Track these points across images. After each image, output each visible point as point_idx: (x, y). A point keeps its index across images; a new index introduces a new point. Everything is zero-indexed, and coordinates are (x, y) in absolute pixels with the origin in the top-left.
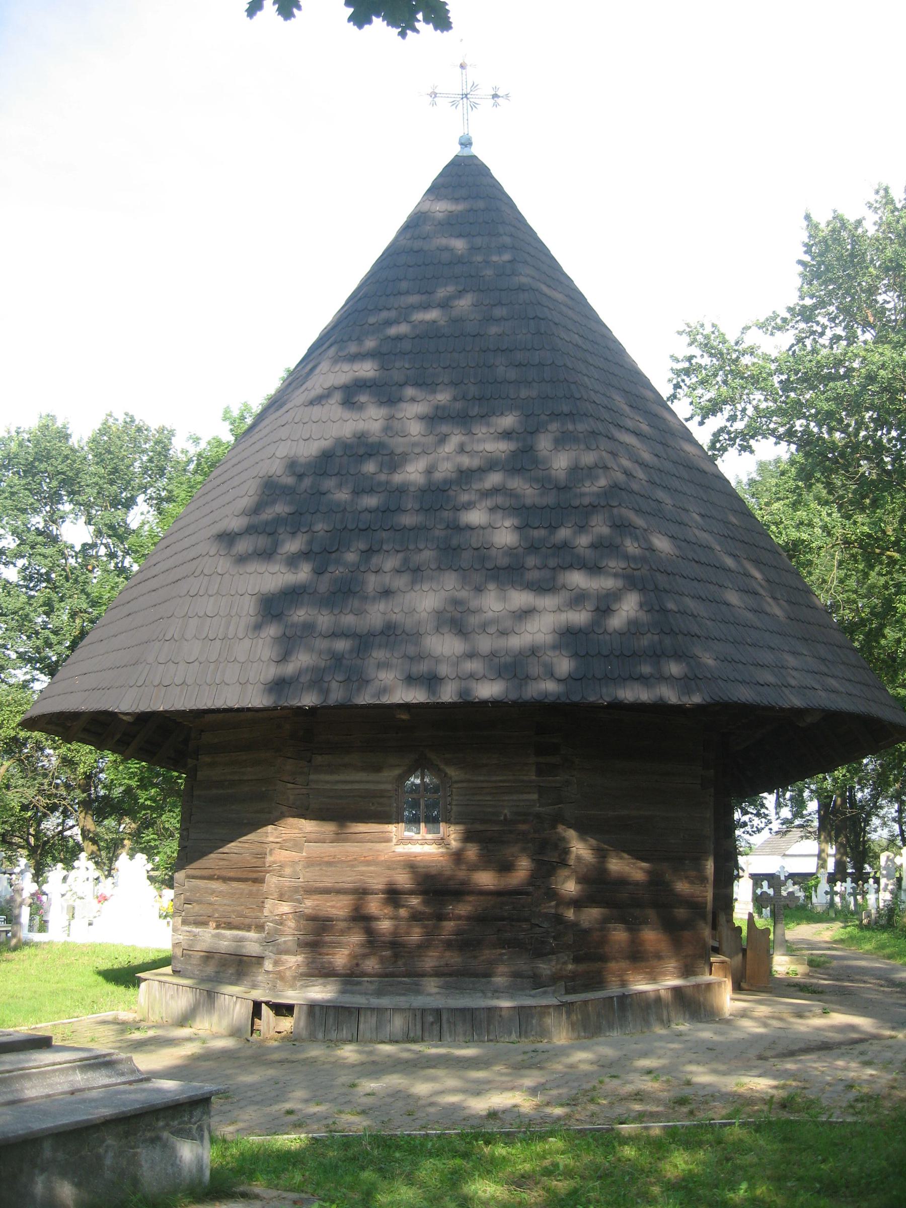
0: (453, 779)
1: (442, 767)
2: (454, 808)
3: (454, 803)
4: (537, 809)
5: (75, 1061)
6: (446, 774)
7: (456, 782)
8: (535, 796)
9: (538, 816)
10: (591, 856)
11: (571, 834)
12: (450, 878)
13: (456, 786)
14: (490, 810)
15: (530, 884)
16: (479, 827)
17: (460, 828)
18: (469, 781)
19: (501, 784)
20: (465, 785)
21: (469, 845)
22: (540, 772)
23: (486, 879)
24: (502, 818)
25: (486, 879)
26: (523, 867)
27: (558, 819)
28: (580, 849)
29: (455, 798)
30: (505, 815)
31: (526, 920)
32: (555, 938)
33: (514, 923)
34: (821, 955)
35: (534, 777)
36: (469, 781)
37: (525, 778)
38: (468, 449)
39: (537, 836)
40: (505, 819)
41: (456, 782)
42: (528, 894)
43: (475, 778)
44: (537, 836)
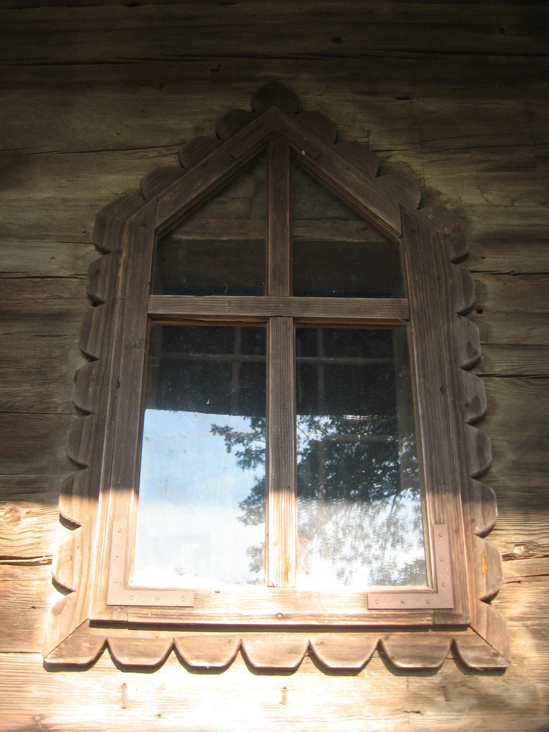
0: (479, 226)
7: (501, 240)
13: (492, 260)
29: (502, 333)
41: (501, 240)
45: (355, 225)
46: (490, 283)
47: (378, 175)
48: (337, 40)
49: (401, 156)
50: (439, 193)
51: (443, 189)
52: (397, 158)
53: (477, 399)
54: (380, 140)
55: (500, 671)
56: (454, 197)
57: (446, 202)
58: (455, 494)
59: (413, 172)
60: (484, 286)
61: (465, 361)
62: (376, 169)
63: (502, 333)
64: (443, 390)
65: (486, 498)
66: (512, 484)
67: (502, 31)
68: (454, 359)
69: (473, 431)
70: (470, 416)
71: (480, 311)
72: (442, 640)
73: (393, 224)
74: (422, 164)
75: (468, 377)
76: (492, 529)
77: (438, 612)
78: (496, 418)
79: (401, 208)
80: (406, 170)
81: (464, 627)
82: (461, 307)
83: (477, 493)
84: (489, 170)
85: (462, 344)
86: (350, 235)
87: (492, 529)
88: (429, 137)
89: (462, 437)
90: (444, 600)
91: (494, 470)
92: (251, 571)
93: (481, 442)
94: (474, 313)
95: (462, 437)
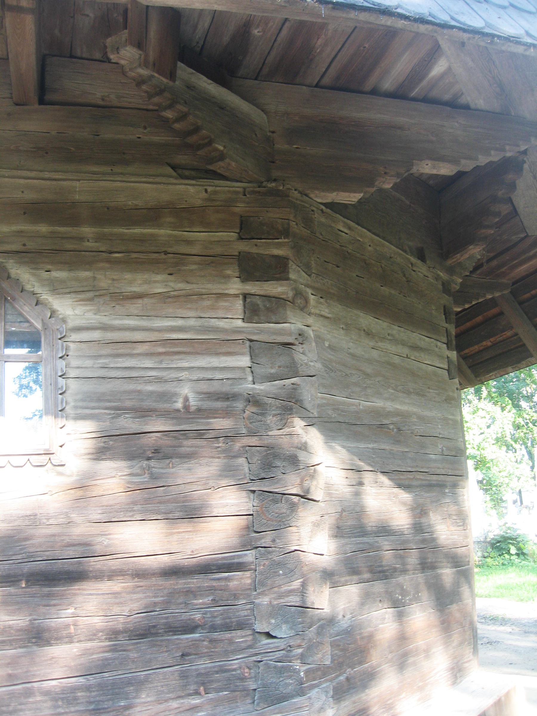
0: (71, 324)
1: (46, 296)
2: (73, 386)
3: (72, 373)
4: (248, 386)
5: (103, 647)
6: (53, 313)
7: (78, 329)
8: (245, 361)
9: (253, 400)
10: (345, 482)
11: (314, 438)
12: (176, 76)
13: (75, 337)
14: (150, 388)
15: (247, 544)
16: (128, 423)
17: (87, 427)
18: (104, 328)
19: (175, 336)
20: (96, 335)
21: (108, 466)
22: (253, 311)
23: (144, 540)
24: (179, 405)
25: (144, 540)
26: (227, 509)
27: (290, 405)
28: (328, 464)
29: (74, 363)
30: (186, 399)
31: (241, 626)
32: (302, 658)
33: (215, 635)
34: (205, 668)
35: (239, 323)
36: (104, 328)
37: (222, 324)
38: (72, 15)
39: (254, 441)
40: (186, 407)
41: (78, 329)
42: (240, 567)
43: (117, 322)
44: (254, 441)
45: (26, 325)
46: (72, 345)
47: (36, 305)
48: (24, 245)
49: (46, 296)
50: (58, 311)
51: (59, 309)
52: (44, 297)
53: (62, 387)
54: (38, 289)
55: (63, 465)
56: (63, 312)
57: (60, 314)
58: (52, 415)
59: (49, 302)
60: (69, 347)
61: (60, 374)
62: (35, 303)
63: (74, 363)
64: (51, 384)
65: (62, 417)
66: (72, 412)
67: (88, 241)
68: (56, 373)
69: (60, 396)
70: (60, 392)
71: (67, 356)
72: (47, 457)
73: (38, 325)
74: (53, 299)
75: (60, 379)
76: (64, 426)
77: (45, 450)
78: (68, 392)
79: (42, 320)
80: (47, 302)
81: (53, 454)
82: (60, 355)
83: (60, 416)
84: (77, 301)
85: (59, 369)
86: (24, 327)
87: (64, 426)
88: (56, 288)
89: (56, 399)
90: (47, 447)
91: (67, 408)
92: (507, 695)
93: (62, 400)
94: (66, 357)
95: (56, 399)
